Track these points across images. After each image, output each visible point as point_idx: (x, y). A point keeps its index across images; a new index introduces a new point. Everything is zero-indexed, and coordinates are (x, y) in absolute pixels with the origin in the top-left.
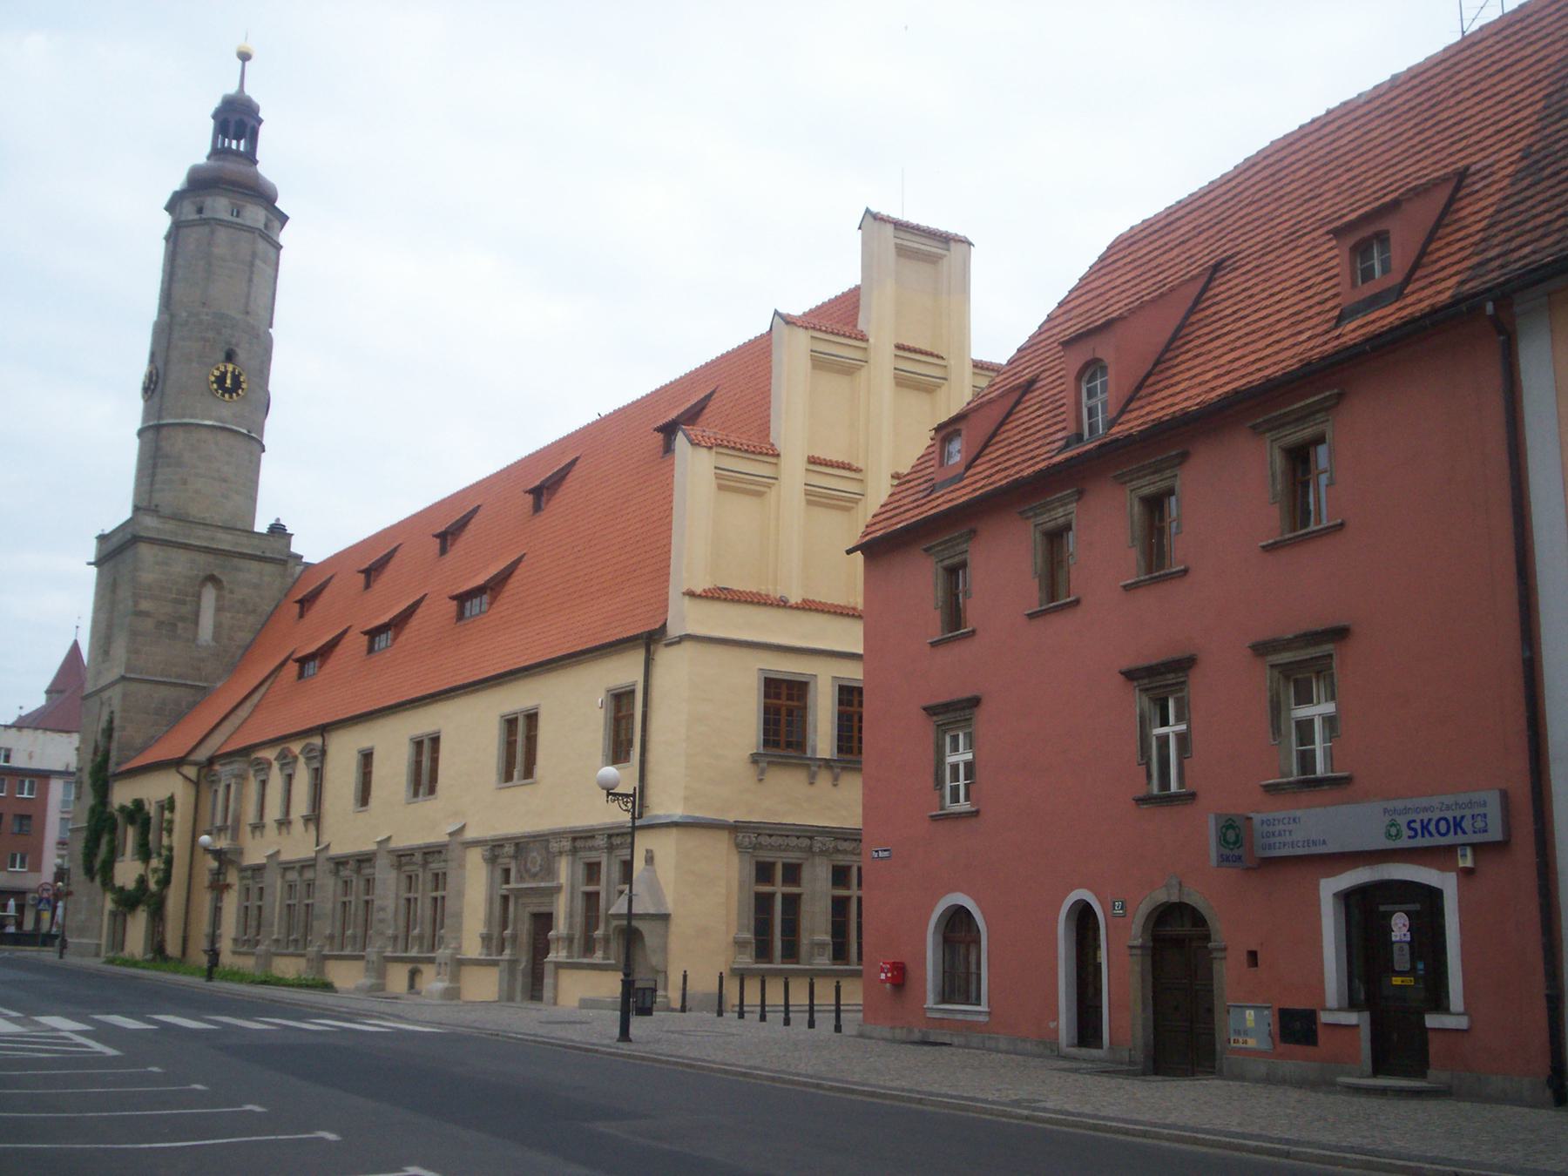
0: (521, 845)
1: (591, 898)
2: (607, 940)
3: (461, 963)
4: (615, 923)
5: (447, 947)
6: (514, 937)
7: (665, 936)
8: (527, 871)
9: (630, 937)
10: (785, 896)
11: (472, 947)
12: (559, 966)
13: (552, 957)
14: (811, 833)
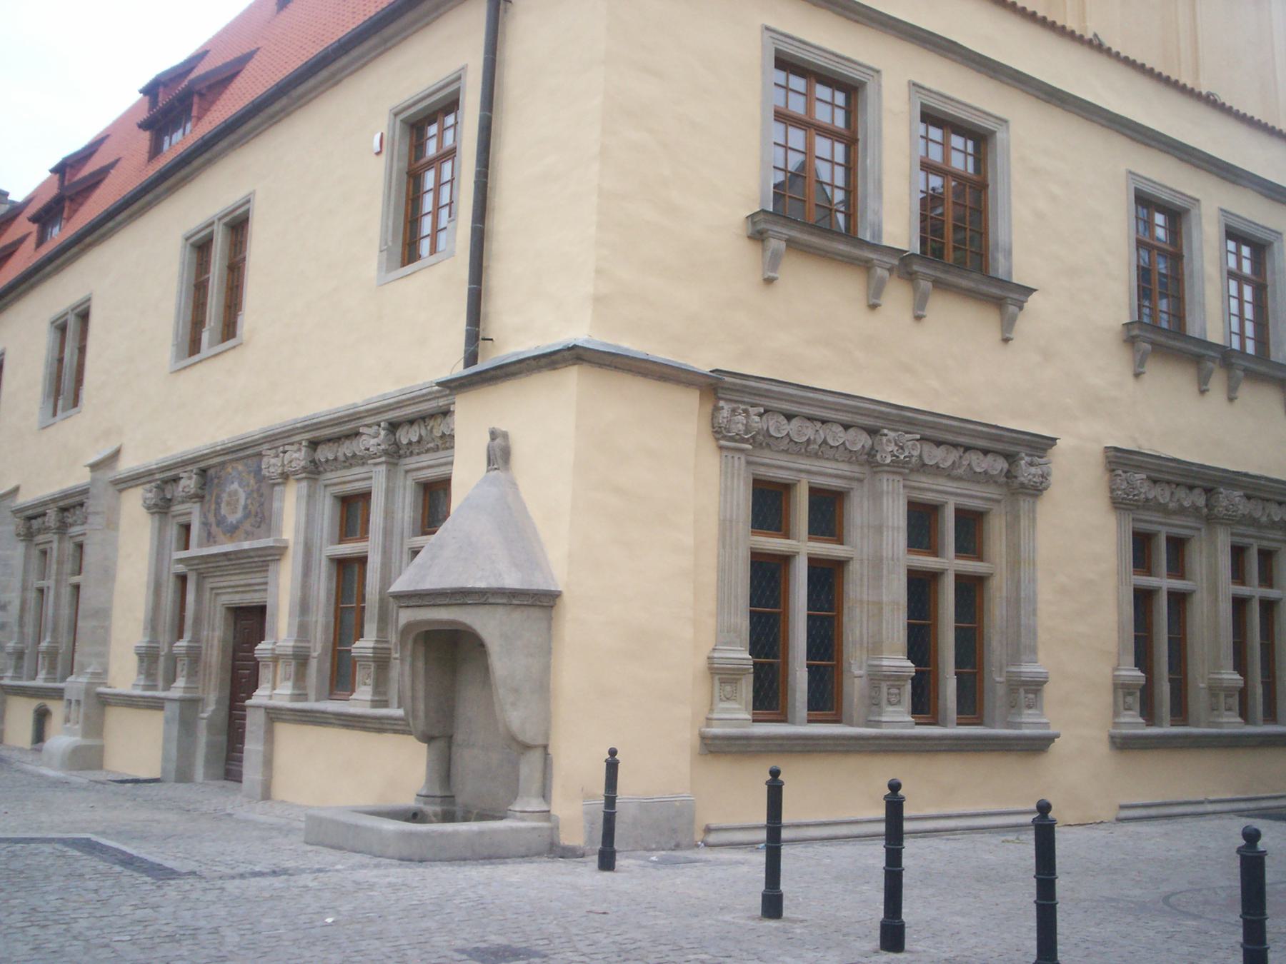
0: (207, 472)
1: (348, 571)
2: (381, 661)
3: (104, 701)
4: (406, 616)
5: (82, 671)
6: (194, 656)
7: (546, 651)
8: (220, 522)
9: (449, 652)
10: (960, 578)
11: (124, 675)
12: (274, 715)
13: (261, 696)
14: (875, 420)
